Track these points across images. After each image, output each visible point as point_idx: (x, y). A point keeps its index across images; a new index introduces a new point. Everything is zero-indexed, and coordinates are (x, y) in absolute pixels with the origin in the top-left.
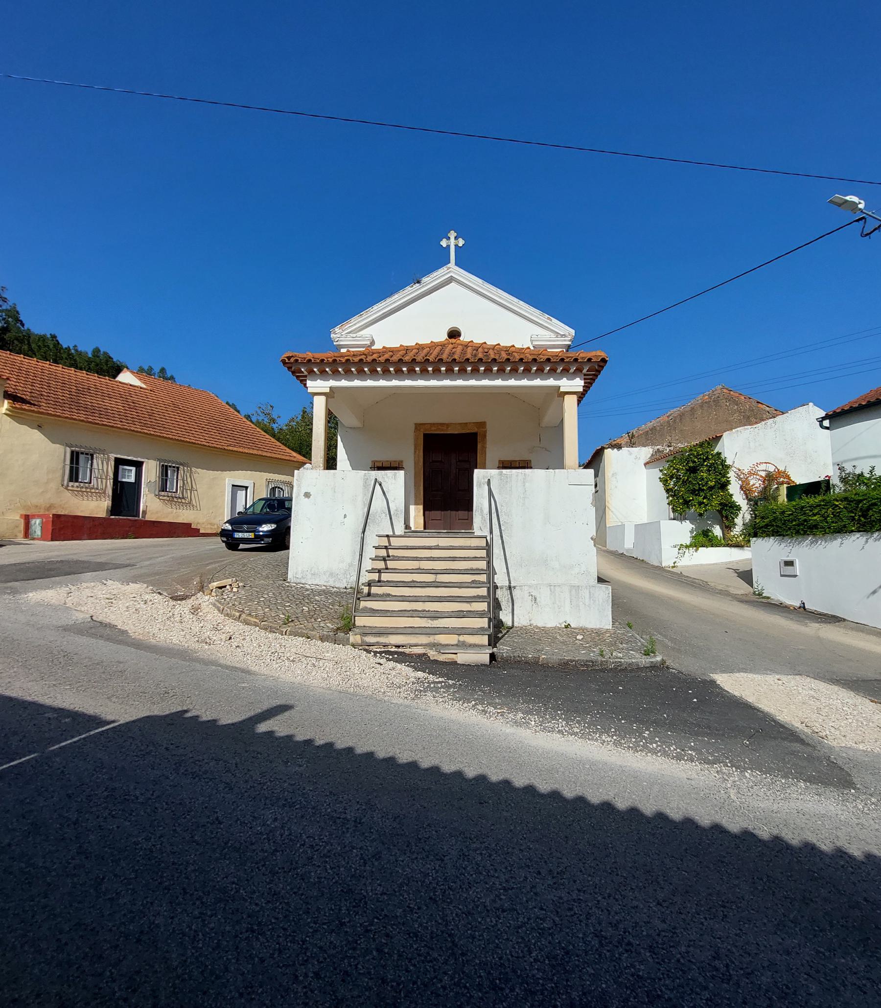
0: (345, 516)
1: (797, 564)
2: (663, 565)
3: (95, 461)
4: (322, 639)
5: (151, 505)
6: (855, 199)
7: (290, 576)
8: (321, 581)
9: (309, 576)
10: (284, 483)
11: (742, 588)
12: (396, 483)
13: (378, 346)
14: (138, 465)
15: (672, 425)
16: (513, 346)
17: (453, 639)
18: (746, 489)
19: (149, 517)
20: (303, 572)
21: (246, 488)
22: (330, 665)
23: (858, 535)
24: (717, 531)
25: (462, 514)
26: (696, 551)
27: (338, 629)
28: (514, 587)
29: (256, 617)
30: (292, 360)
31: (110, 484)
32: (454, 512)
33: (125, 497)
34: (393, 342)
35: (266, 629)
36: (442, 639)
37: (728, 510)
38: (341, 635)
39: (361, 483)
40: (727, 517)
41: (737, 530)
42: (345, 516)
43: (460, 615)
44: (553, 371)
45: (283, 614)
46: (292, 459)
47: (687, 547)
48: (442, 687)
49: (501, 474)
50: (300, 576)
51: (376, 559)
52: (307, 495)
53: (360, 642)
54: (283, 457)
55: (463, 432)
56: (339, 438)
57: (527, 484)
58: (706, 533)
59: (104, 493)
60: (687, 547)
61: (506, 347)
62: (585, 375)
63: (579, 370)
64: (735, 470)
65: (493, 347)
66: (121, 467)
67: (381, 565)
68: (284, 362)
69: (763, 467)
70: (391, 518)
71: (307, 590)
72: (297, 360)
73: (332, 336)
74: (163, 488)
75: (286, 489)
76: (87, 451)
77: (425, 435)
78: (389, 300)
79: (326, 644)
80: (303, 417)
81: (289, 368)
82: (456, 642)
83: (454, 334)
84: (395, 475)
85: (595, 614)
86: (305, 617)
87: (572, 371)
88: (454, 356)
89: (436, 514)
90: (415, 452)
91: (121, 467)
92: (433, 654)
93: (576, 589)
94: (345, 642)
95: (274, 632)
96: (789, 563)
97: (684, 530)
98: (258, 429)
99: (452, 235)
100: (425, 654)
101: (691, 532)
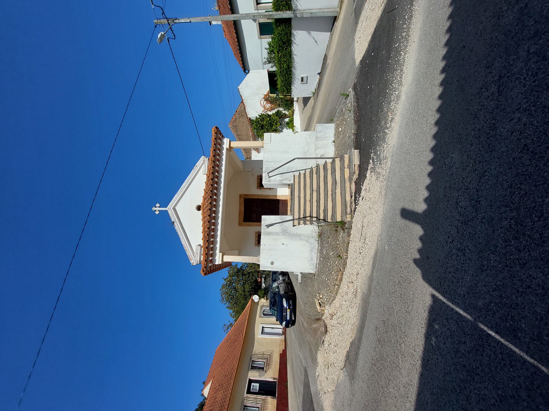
0: (283, 244)
1: (302, 76)
3: (248, 405)
4: (349, 235)
5: (270, 375)
6: (160, 35)
8: (315, 256)
11: (311, 102)
13: (201, 243)
14: (251, 381)
17: (347, 171)
18: (272, 109)
19: (277, 376)
20: (310, 265)
21: (263, 327)
23: (292, 47)
24: (287, 120)
25: (281, 206)
31: (260, 397)
33: (267, 389)
36: (347, 175)
39: (267, 236)
42: (283, 244)
52: (272, 263)
58: (288, 123)
59: (264, 400)
66: (251, 391)
68: (205, 274)
69: (262, 102)
72: (205, 267)
74: (262, 368)
76: (242, 409)
78: (181, 237)
82: (348, 169)
83: (199, 208)
85: (329, 130)
91: (251, 391)
92: (355, 177)
94: (351, 222)
96: (302, 79)
99: (154, 209)
100: (355, 182)
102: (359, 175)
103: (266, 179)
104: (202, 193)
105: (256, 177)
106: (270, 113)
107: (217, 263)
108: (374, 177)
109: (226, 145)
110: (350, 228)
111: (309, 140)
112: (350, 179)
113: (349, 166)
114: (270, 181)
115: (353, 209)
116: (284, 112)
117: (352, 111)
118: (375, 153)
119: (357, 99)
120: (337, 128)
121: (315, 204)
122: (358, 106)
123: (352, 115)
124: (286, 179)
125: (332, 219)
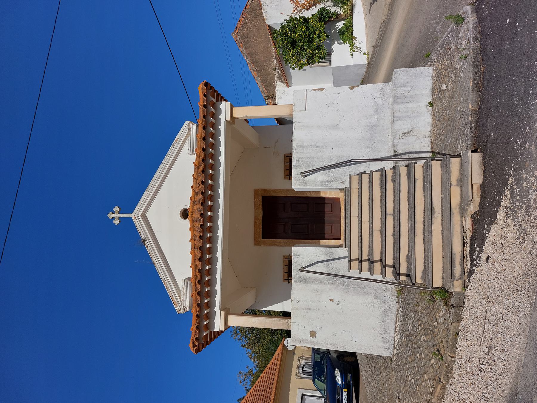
0: (331, 300)
2: (366, 63)
4: (458, 320)
7: (386, 354)
8: (392, 324)
9: (387, 336)
10: (299, 364)
12: (303, 254)
15: (260, 68)
16: (194, 163)
17: (455, 192)
20: (383, 342)
21: (303, 395)
22: (493, 309)
24: (340, 25)
25: (327, 209)
26: (355, 38)
27: (446, 304)
28: (395, 151)
29: (434, 387)
30: (196, 343)
32: (326, 215)
34: (188, 259)
35: (448, 378)
36: (455, 200)
37: (325, 17)
38: (453, 301)
39: (302, 285)
40: (330, 17)
41: (339, 10)
42: (331, 300)
43: (428, 187)
44: (213, 125)
45: (430, 360)
46: (280, 356)
47: (352, 45)
48: (520, 187)
49: (296, 166)
50: (387, 346)
51: (371, 270)
52: (313, 334)
53: (461, 282)
54: (279, 362)
55: (261, 207)
56: (264, 309)
57: (305, 144)
58: (342, 33)
60: (352, 45)
61: (195, 168)
62: (217, 101)
63: (213, 105)
64: (294, 14)
65: (195, 179)
67: (377, 266)
68: (197, 351)
70: (333, 260)
71: (401, 338)
73: (182, 313)
75: (304, 362)
77: (263, 238)
78: (157, 265)
79: (464, 315)
80: (249, 347)
81: (203, 346)
82: (458, 189)
83: (185, 214)
84: (296, 255)
85: (420, 81)
86: (433, 338)
87: (213, 110)
88: (201, 214)
89: (327, 228)
90: (277, 245)
92: (473, 208)
93: (396, 99)
94: (462, 297)
95: (452, 369)
97: (340, 53)
98: (257, 383)
99: (111, 215)
100: (472, 217)
101: (341, 44)
102: (481, 205)
103: (298, 180)
104: (191, 182)
105: (282, 158)
106: (308, 14)
107: (217, 329)
108: (512, 235)
109: (224, 116)
110: (462, 306)
111: (380, 101)
112: (463, 209)
113: (461, 183)
114: (305, 184)
115: (467, 270)
116: (333, 9)
117: (470, 60)
118: (518, 181)
119: (482, 33)
120: (438, 78)
121: (390, 240)
122: (483, 51)
123: (468, 65)
124: (335, 180)
125: (423, 278)
